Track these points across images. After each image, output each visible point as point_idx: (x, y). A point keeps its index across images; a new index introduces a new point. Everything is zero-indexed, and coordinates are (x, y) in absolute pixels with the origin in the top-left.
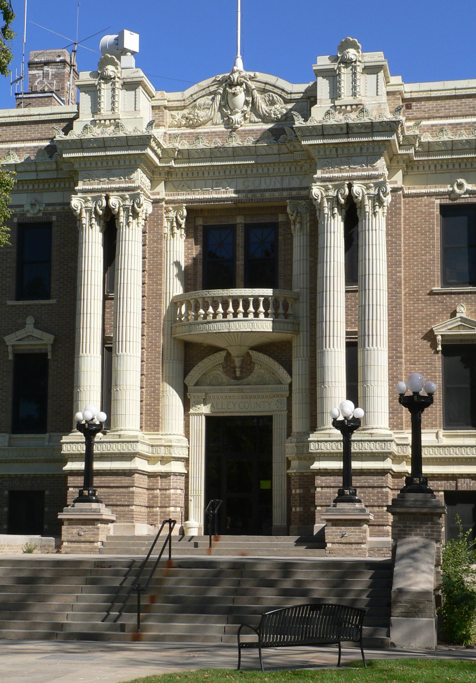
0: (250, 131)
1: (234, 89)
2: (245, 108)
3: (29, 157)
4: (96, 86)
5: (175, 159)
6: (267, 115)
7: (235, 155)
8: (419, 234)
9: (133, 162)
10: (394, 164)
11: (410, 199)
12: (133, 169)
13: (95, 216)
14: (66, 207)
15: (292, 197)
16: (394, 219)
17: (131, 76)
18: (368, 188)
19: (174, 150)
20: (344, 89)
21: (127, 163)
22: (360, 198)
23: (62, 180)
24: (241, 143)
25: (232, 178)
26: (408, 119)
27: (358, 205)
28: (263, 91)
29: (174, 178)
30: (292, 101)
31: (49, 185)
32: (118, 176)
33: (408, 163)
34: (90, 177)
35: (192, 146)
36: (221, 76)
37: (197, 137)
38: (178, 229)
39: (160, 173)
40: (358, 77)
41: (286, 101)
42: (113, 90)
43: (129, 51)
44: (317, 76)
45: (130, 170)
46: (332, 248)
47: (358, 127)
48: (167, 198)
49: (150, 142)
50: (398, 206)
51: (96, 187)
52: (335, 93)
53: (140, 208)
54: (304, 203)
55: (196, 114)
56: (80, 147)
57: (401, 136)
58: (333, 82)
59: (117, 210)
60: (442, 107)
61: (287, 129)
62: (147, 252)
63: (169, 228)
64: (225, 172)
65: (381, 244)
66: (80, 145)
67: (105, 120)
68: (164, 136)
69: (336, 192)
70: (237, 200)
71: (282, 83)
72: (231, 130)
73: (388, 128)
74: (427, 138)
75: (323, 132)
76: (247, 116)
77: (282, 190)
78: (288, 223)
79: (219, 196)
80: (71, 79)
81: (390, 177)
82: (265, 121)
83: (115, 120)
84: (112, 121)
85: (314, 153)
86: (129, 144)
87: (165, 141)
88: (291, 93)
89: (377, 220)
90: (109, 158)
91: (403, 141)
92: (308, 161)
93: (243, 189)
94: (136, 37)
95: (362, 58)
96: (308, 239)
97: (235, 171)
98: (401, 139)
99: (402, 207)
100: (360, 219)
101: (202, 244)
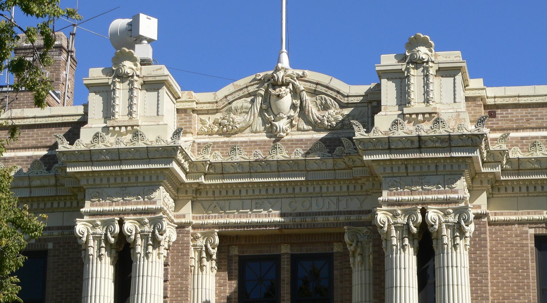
0: (298, 140)
1: (278, 90)
2: (292, 113)
3: (21, 170)
4: (110, 86)
5: (205, 174)
6: (319, 121)
7: (280, 170)
8: (510, 271)
9: (154, 179)
10: (477, 184)
11: (497, 227)
12: (154, 187)
13: (106, 245)
14: (66, 232)
15: (350, 223)
16: (478, 252)
17: (153, 74)
18: (446, 214)
19: (204, 163)
20: (415, 95)
21: (147, 179)
22: (437, 227)
23: (62, 198)
24: (287, 156)
25: (275, 198)
26: (493, 130)
27: (434, 236)
28: (314, 93)
29: (203, 197)
30: (349, 105)
31: (45, 205)
32: (136, 195)
33: (494, 182)
34: (101, 196)
35: (226, 158)
36: (262, 74)
37: (233, 147)
38: (208, 261)
39: (187, 191)
40: (431, 81)
41: (343, 106)
42: (131, 90)
43: (146, 39)
44: (380, 78)
45: (151, 188)
46: (403, 288)
47: (433, 141)
48: (194, 222)
49: (176, 155)
50: (482, 236)
51: (107, 208)
52: (403, 99)
53: (162, 235)
54: (366, 230)
55: (231, 119)
56: (89, 160)
57: (485, 152)
58: (401, 86)
59: (133, 237)
60: (533, 116)
61: (344, 141)
62: (169, 289)
63: (197, 260)
64: (267, 190)
65: (463, 284)
66: (89, 157)
67: (120, 127)
68: (193, 146)
69: (406, 219)
70: (281, 225)
71: (337, 84)
72: (274, 139)
73: (469, 143)
74: (516, 153)
75: (389, 146)
76: (294, 122)
77: (338, 214)
78: (345, 255)
79: (260, 220)
80: (68, 67)
81: (472, 199)
82: (317, 128)
83: (132, 126)
84: (129, 128)
85: (378, 171)
86: (150, 157)
87: (193, 152)
88: (348, 96)
89: (459, 255)
90: (125, 173)
91: (486, 157)
92: (371, 179)
93: (290, 212)
94: (154, 21)
95: (436, 58)
96: (371, 275)
97: (280, 189)
98: (485, 155)
99: (488, 237)
100: (437, 252)
101: (237, 278)
